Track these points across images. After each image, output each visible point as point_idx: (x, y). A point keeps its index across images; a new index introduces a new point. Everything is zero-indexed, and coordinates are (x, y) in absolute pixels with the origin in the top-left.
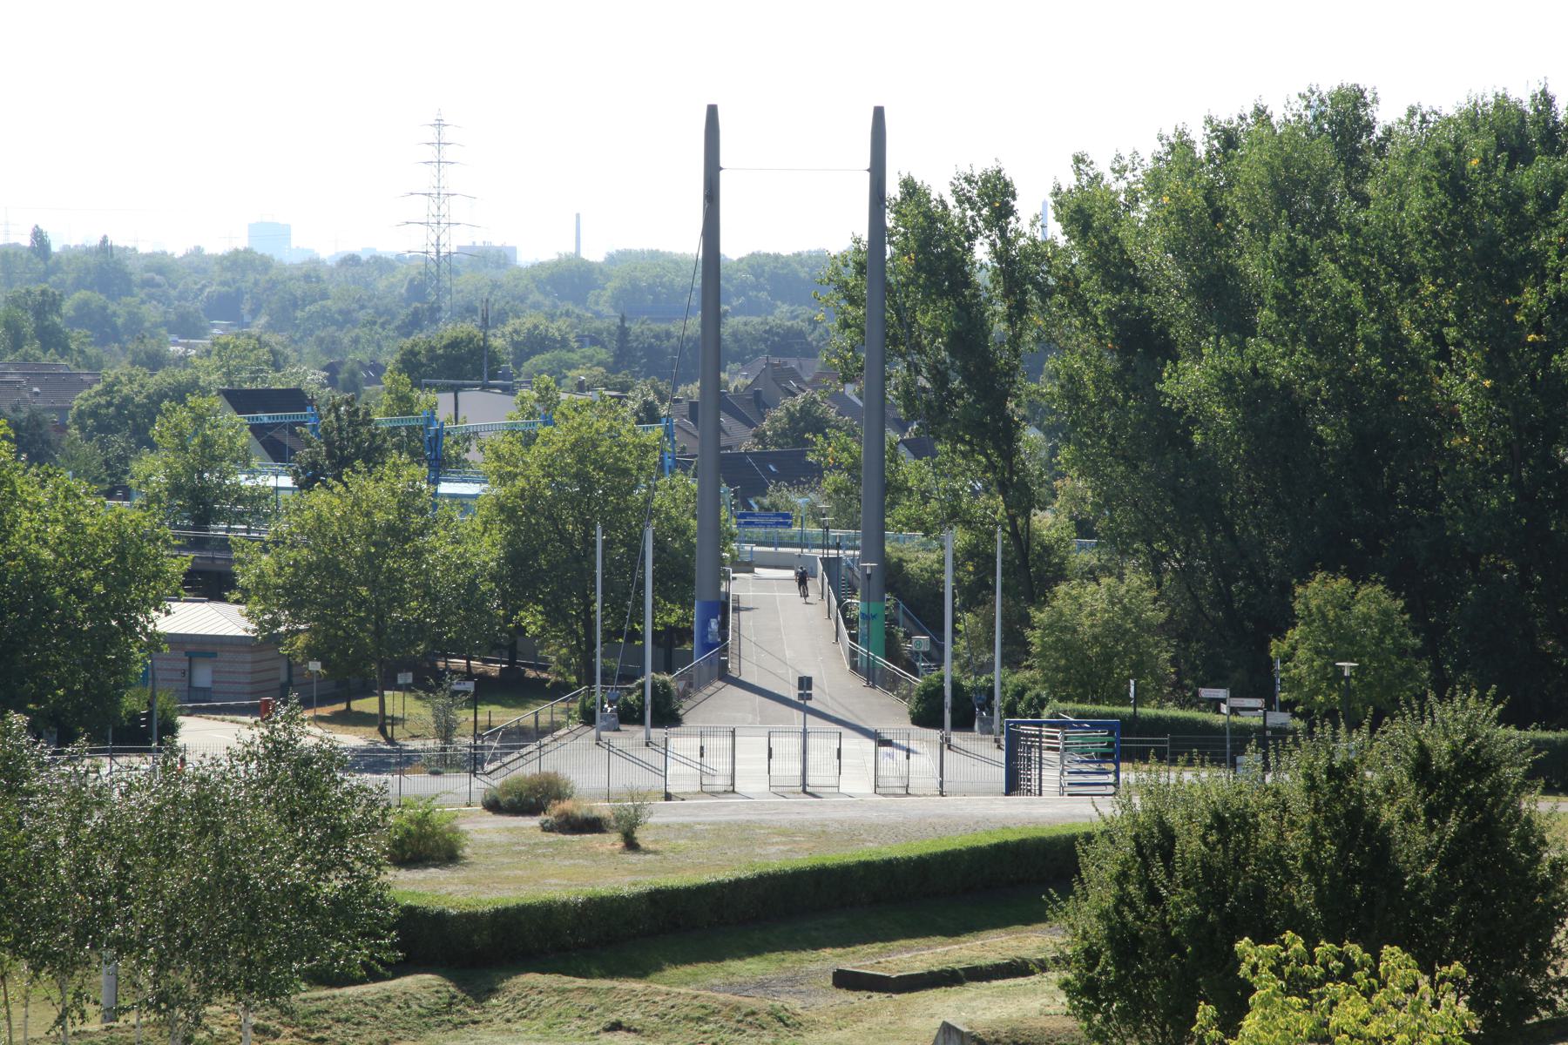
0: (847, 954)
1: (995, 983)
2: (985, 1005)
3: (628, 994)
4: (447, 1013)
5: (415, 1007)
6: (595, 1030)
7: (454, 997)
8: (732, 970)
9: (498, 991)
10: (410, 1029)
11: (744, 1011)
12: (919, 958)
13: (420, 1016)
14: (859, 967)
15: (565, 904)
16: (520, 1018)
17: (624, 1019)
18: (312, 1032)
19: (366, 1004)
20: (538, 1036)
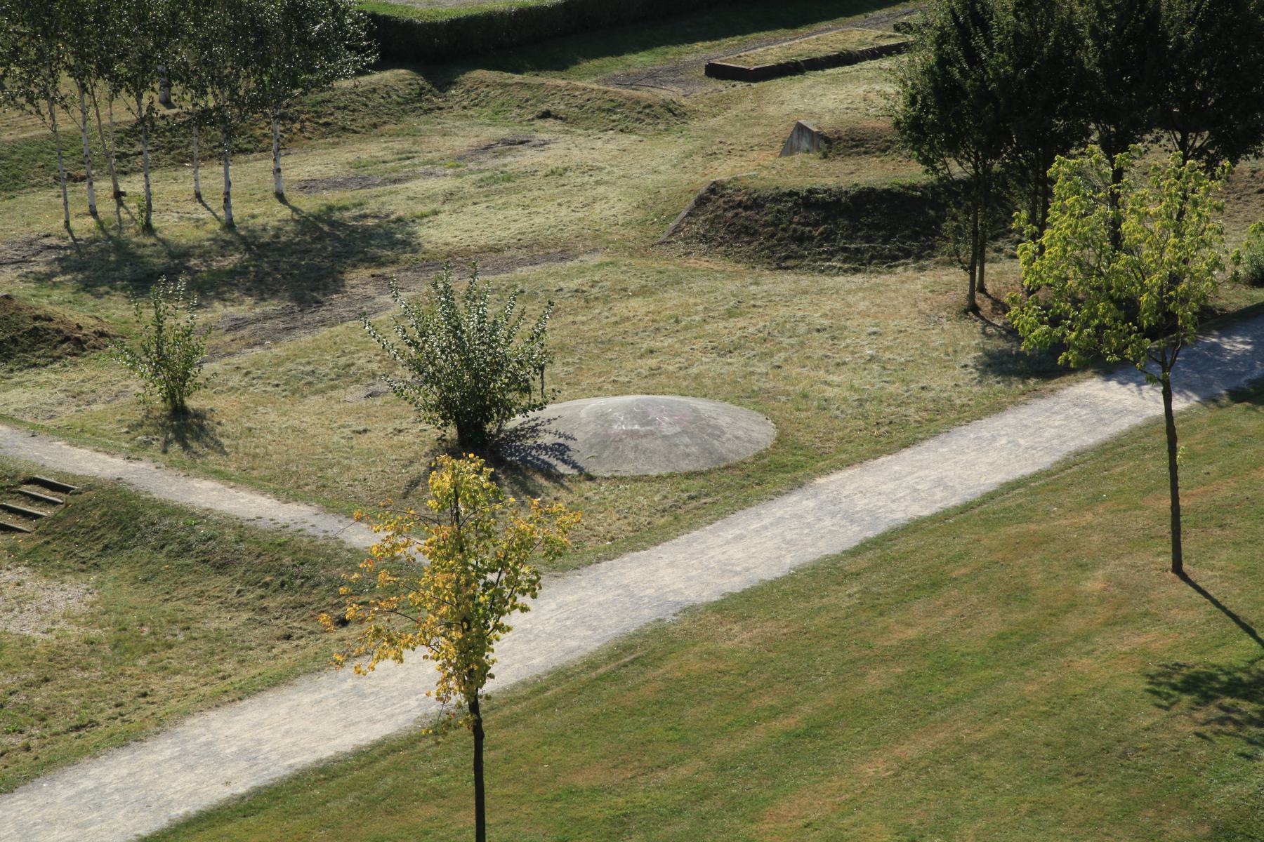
0: (714, 46)
1: (828, 71)
2: (821, 92)
3: (554, 89)
4: (418, 101)
5: (394, 97)
6: (530, 117)
7: (423, 88)
8: (628, 62)
9: (455, 83)
10: (392, 114)
11: (643, 104)
12: (770, 51)
13: (399, 104)
14: (725, 61)
15: (502, 14)
16: (474, 106)
17: (552, 109)
18: (320, 117)
19: (358, 95)
20: (488, 121)
